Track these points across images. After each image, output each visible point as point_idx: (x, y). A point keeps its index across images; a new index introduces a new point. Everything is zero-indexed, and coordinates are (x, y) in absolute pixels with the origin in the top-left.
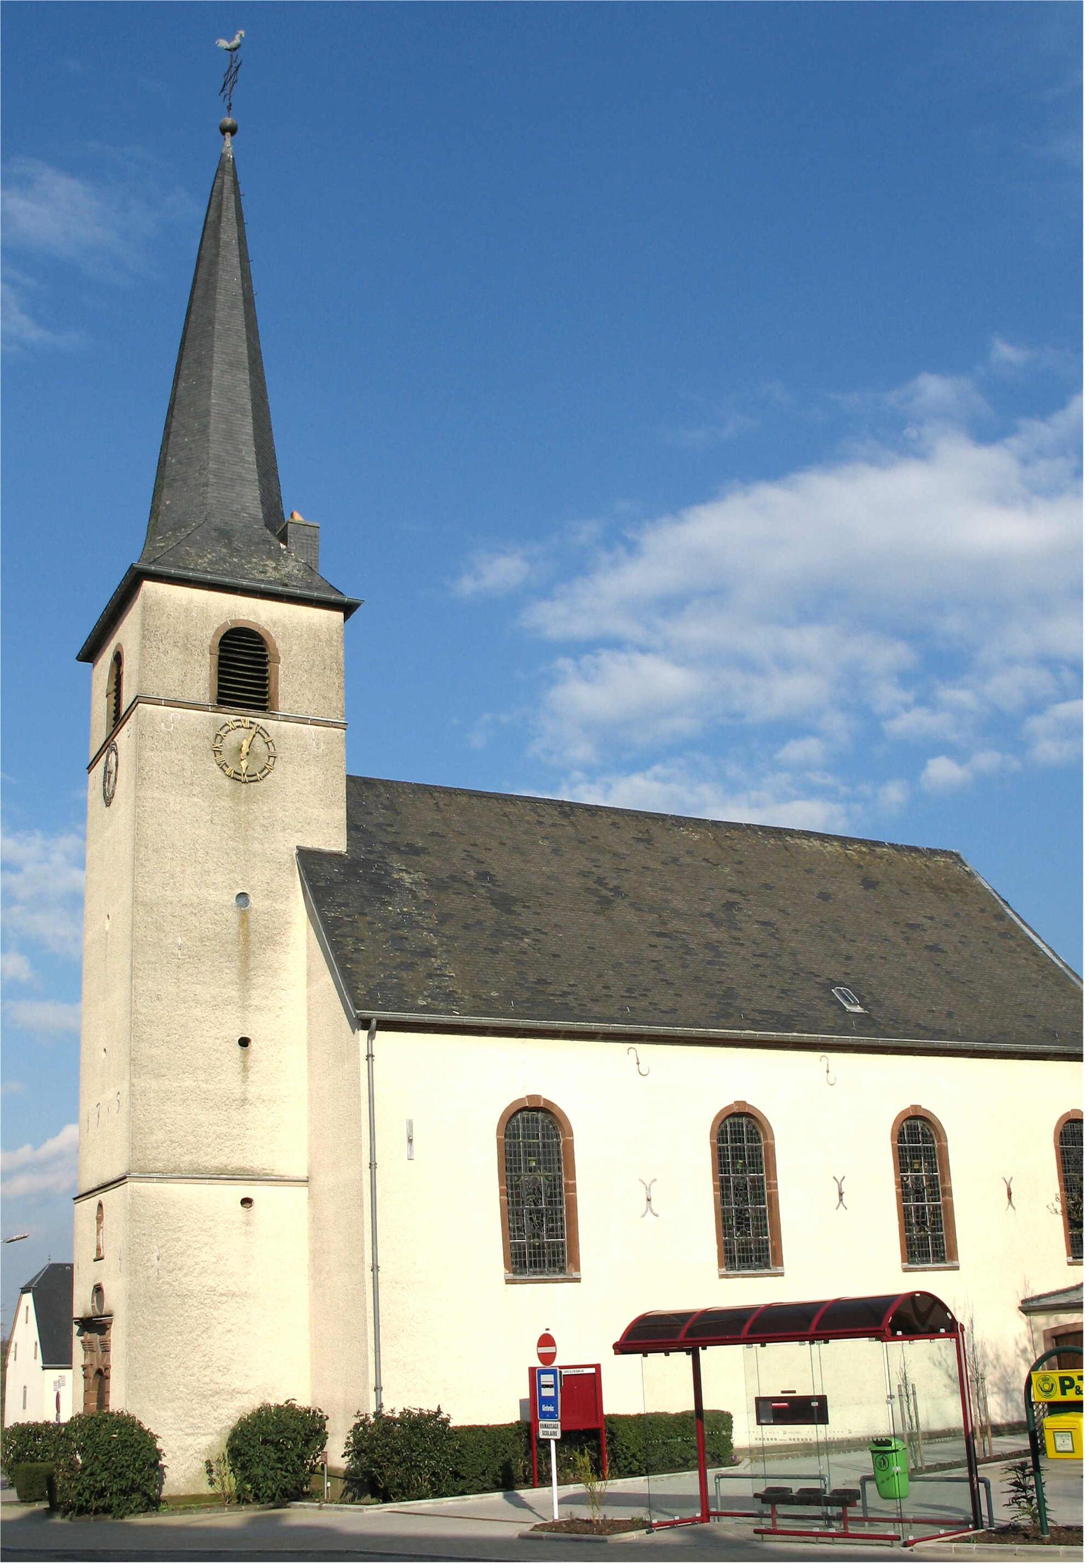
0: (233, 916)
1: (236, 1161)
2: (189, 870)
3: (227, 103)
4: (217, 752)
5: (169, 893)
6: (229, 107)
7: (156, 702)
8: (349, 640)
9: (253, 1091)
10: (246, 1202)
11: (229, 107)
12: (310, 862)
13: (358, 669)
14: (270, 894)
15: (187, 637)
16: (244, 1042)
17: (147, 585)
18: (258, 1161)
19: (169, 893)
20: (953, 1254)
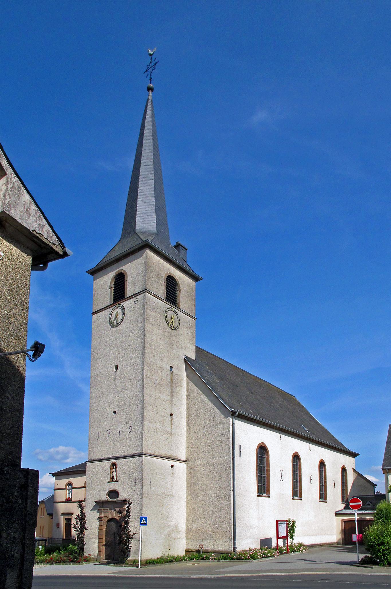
0: (169, 372)
1: (169, 453)
2: (159, 355)
3: (149, 77)
4: (166, 317)
5: (153, 361)
6: (151, 79)
7: (150, 293)
8: (197, 287)
9: (173, 432)
10: (172, 466)
11: (151, 79)
12: (187, 360)
13: (199, 297)
14: (178, 368)
15: (158, 273)
16: (171, 415)
17: (148, 252)
18: (174, 454)
19: (153, 361)
20: (268, 491)
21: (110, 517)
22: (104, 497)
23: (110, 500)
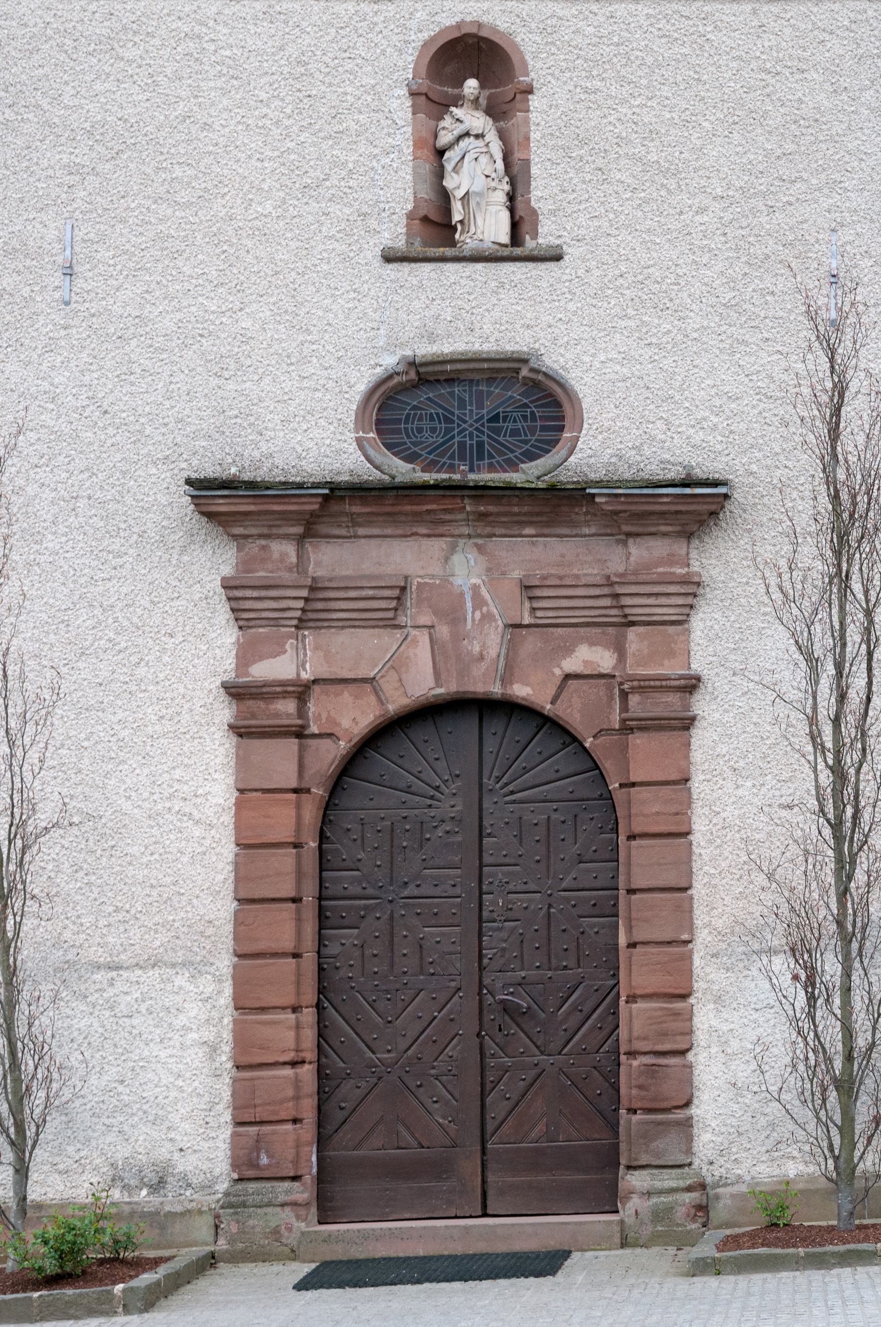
21: (421, 682)
22: (327, 443)
23: (403, 470)
